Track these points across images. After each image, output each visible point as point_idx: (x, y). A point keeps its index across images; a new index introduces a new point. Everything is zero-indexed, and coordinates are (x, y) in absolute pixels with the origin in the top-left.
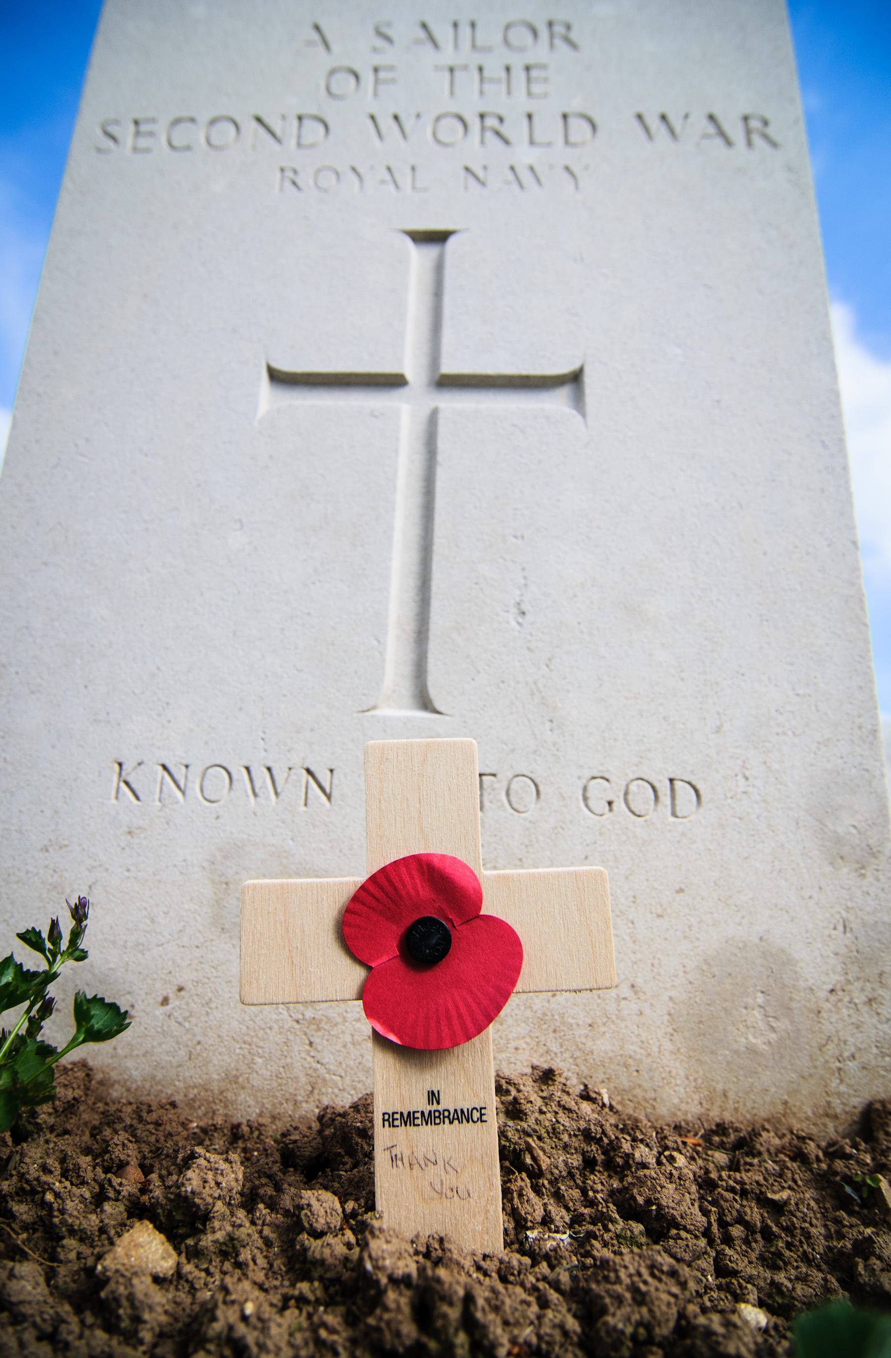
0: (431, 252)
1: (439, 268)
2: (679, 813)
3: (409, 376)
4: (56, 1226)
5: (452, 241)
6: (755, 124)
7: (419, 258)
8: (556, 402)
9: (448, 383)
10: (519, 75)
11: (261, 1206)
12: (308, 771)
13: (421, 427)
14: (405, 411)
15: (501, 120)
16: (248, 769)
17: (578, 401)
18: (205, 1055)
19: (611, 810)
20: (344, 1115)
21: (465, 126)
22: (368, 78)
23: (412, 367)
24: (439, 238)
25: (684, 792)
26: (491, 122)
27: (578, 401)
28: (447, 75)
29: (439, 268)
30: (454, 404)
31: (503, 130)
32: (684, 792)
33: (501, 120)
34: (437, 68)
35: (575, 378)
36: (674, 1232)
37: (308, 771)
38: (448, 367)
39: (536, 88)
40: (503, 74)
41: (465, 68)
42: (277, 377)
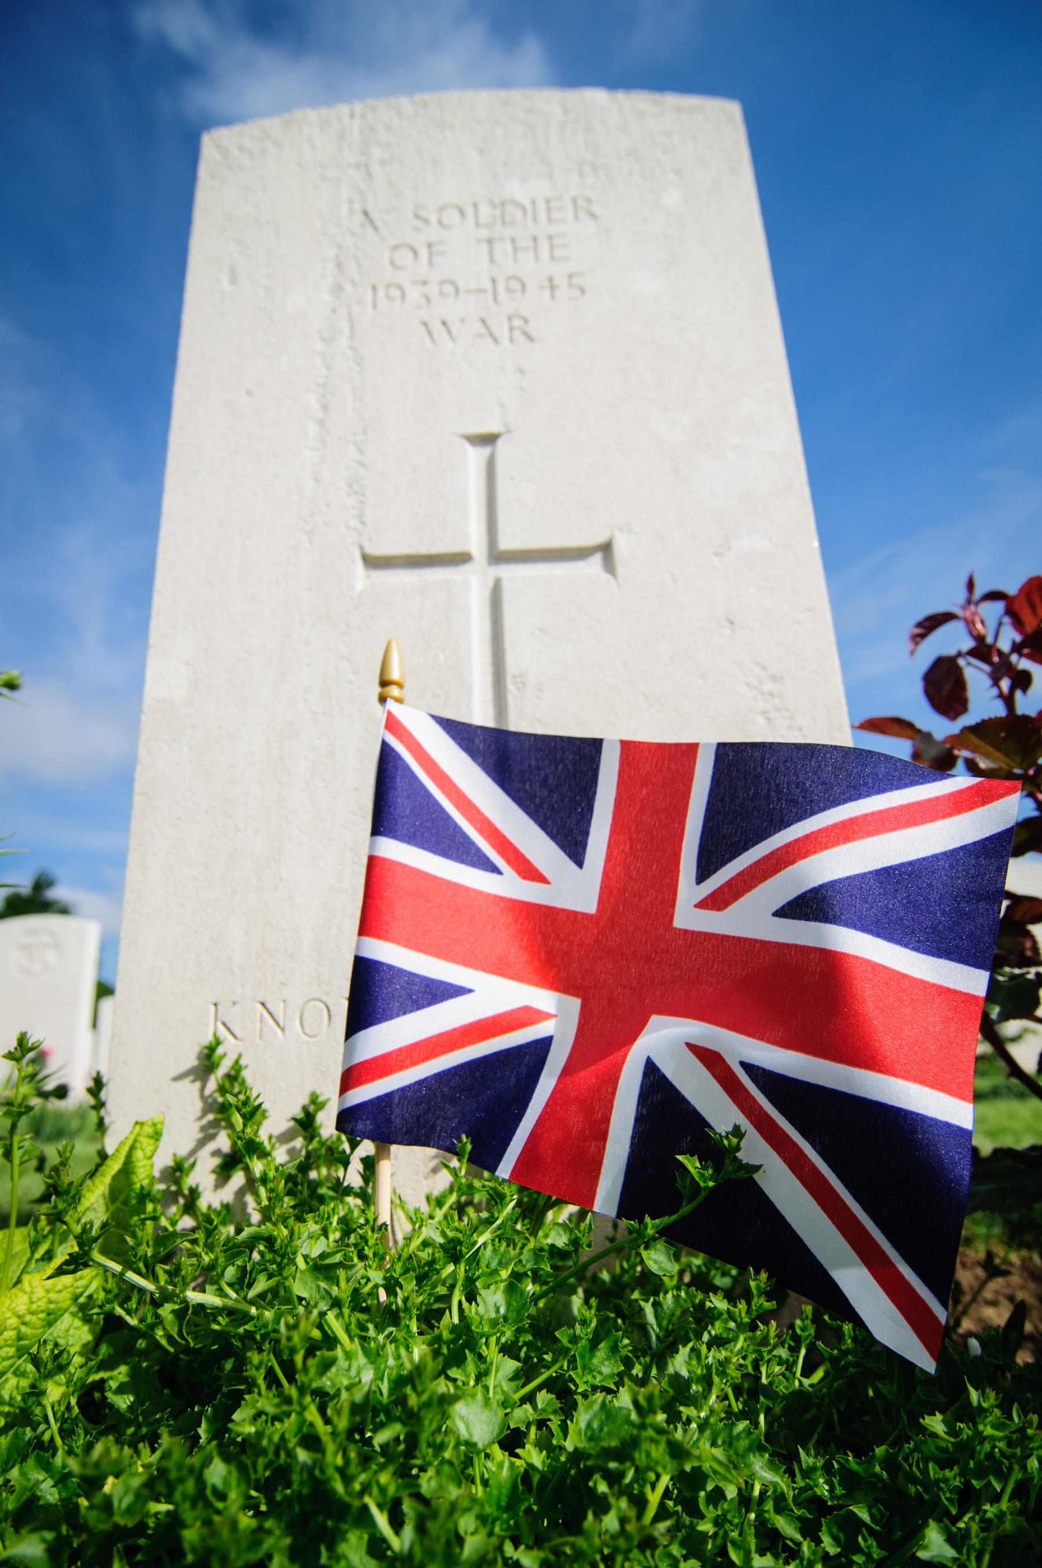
0: (485, 452)
4: (843, 1321)
5: (500, 442)
7: (476, 455)
9: (498, 557)
10: (544, 245)
11: (75, 1545)
13: (487, 593)
14: (473, 583)
17: (609, 565)
20: (488, 1544)
22: (424, 253)
23: (476, 544)
24: (489, 440)
27: (609, 565)
28: (485, 247)
30: (509, 572)
34: (479, 241)
35: (606, 549)
36: (104, 1350)
38: (505, 543)
39: (558, 253)
40: (530, 244)
41: (502, 239)
42: (372, 562)
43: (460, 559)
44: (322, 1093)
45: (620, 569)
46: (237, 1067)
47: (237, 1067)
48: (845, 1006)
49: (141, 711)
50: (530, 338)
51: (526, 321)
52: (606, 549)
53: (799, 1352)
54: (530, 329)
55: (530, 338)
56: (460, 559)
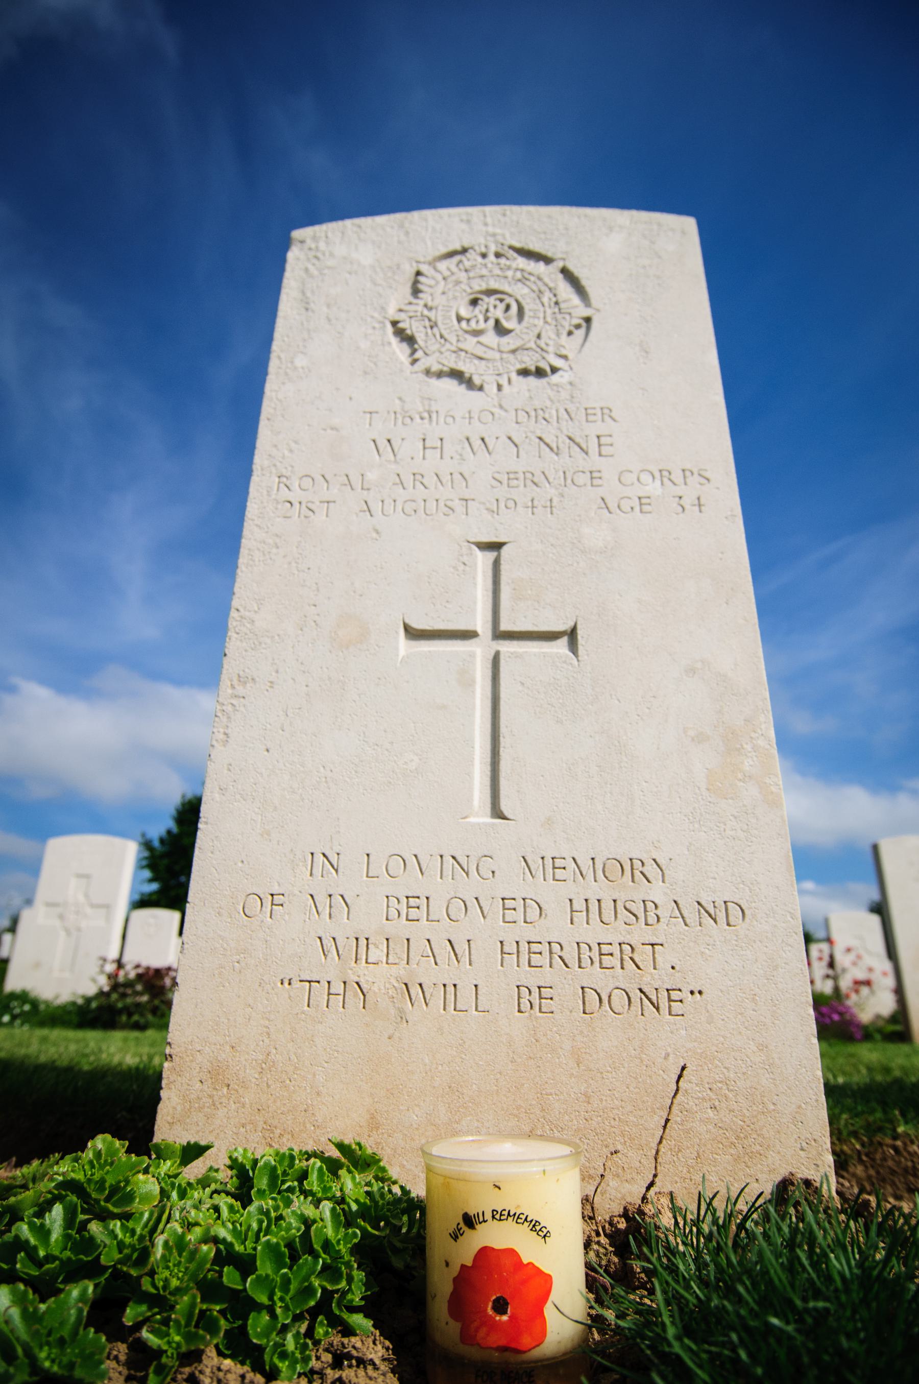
0: (492, 555)
1: (496, 564)
2: (731, 923)
3: (479, 631)
5: (505, 549)
6: (665, 473)
7: (483, 560)
8: (561, 647)
9: (500, 635)
12: (324, 855)
14: (479, 651)
15: (423, 476)
16: (476, 898)
18: (467, 1099)
19: (493, 876)
21: (654, 478)
23: (481, 622)
24: (496, 546)
25: (734, 911)
26: (418, 477)
29: (496, 564)
30: (507, 648)
31: (424, 481)
32: (734, 911)
33: (423, 476)
37: (324, 855)
38: (504, 626)
43: (468, 635)
44: (412, 1191)
45: (581, 650)
46: (340, 1146)
47: (340, 1146)
48: (501, 1306)
49: (237, 567)
50: (614, 420)
51: (611, 410)
52: (572, 634)
53: (692, 1288)
54: (613, 414)
55: (614, 420)
56: (468, 635)
